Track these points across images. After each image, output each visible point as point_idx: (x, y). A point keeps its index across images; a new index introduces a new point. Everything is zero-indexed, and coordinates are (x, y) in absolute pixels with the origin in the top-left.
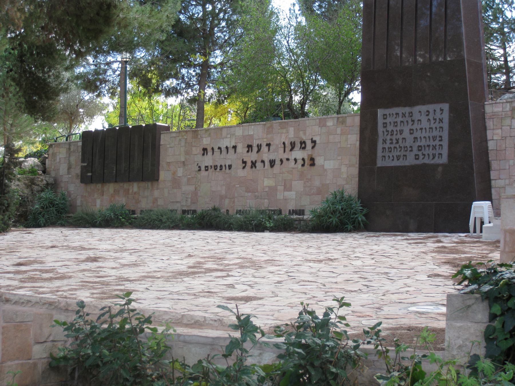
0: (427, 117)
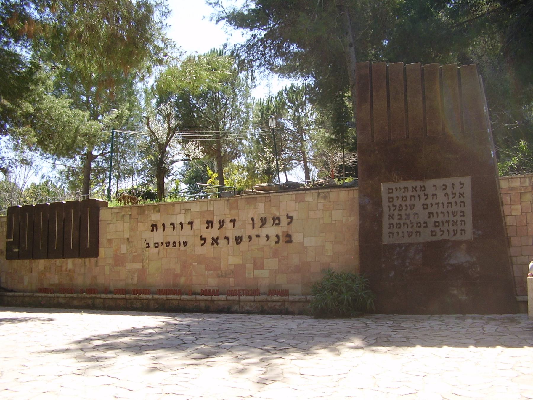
0: (445, 191)
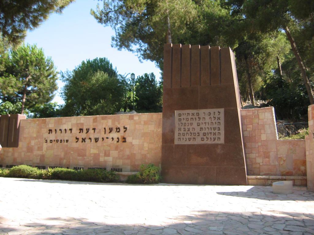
0: (210, 116)
